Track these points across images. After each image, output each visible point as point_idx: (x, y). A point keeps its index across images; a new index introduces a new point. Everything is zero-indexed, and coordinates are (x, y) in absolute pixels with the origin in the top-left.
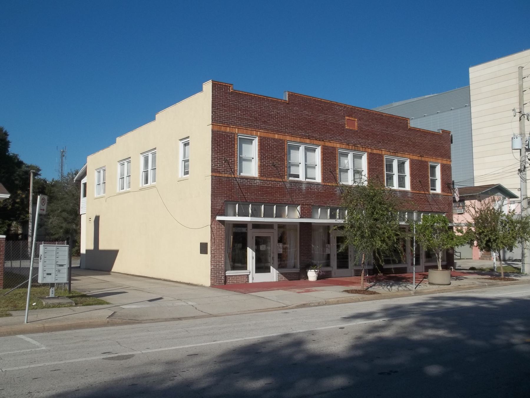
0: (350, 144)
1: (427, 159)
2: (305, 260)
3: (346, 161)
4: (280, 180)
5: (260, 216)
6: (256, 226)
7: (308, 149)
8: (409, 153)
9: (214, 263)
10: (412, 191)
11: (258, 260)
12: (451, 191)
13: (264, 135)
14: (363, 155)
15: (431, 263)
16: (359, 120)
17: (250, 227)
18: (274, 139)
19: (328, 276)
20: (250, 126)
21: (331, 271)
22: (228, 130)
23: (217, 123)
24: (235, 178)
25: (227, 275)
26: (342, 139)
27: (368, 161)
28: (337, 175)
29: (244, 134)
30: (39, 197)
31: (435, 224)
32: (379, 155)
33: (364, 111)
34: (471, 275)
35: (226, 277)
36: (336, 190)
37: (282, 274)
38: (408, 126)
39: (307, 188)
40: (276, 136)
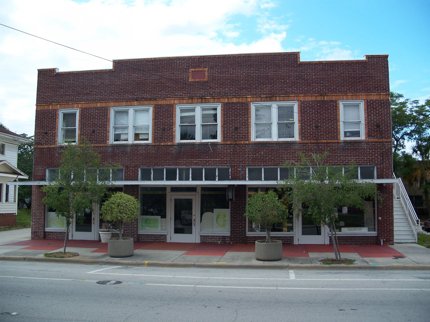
6: (175, 189)
9: (34, 220)
13: (85, 106)
16: (212, 68)
17: (168, 190)
21: (292, 237)
23: (41, 103)
28: (174, 133)
29: (65, 109)
30: (47, 172)
31: (312, 181)
35: (45, 232)
40: (99, 105)
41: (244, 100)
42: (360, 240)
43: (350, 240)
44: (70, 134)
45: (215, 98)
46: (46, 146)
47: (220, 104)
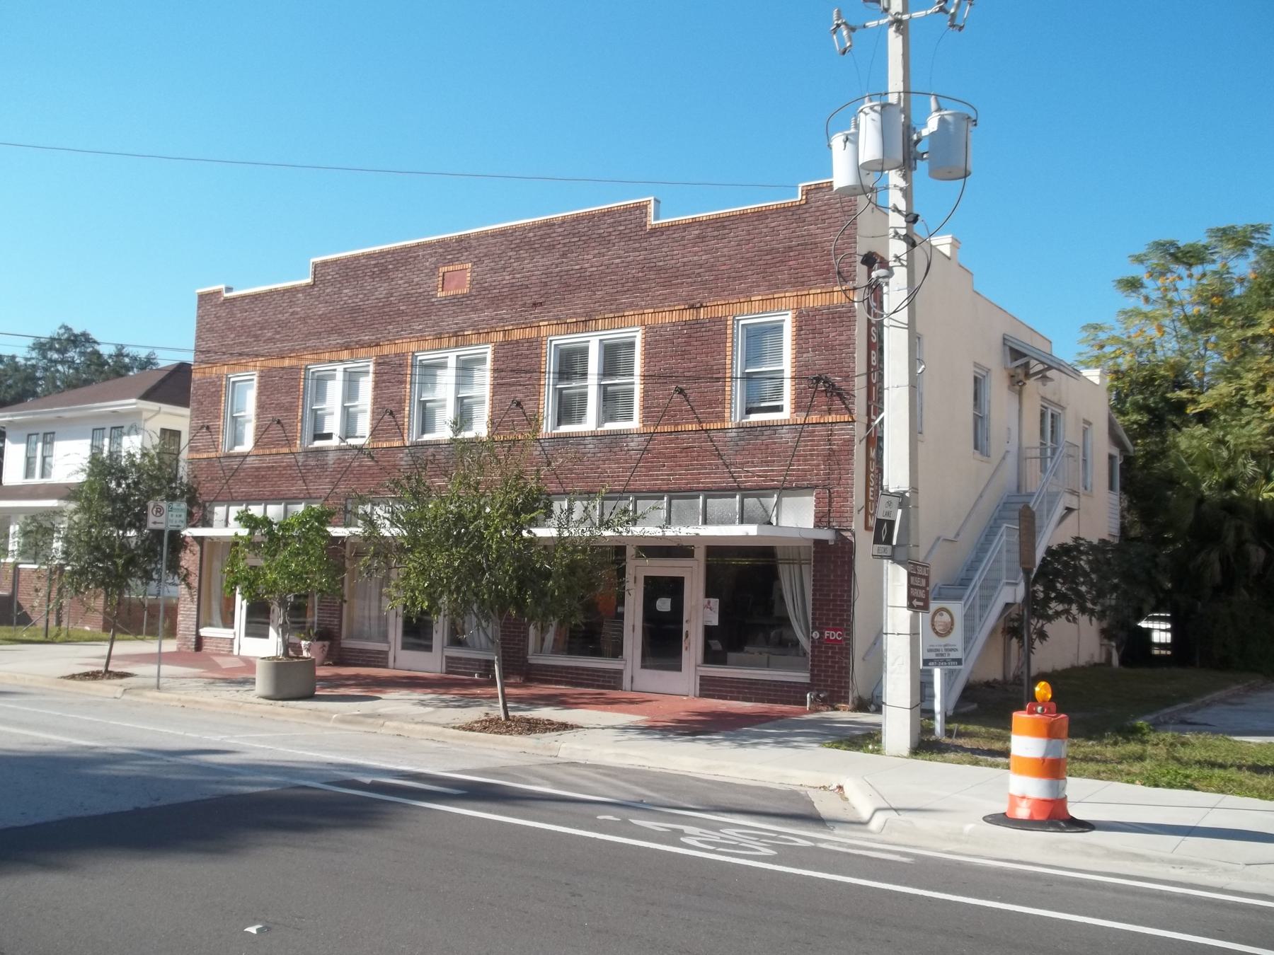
1: (720, 312)
4: (286, 450)
10: (255, 452)
11: (251, 612)
12: (844, 403)
15: (748, 671)
18: (283, 368)
19: (378, 662)
22: (702, 314)
32: (529, 341)
34: (733, 709)
41: (533, 333)
42: (769, 690)
43: (747, 688)
44: (612, 402)
45: (482, 333)
46: (205, 456)
47: (490, 346)
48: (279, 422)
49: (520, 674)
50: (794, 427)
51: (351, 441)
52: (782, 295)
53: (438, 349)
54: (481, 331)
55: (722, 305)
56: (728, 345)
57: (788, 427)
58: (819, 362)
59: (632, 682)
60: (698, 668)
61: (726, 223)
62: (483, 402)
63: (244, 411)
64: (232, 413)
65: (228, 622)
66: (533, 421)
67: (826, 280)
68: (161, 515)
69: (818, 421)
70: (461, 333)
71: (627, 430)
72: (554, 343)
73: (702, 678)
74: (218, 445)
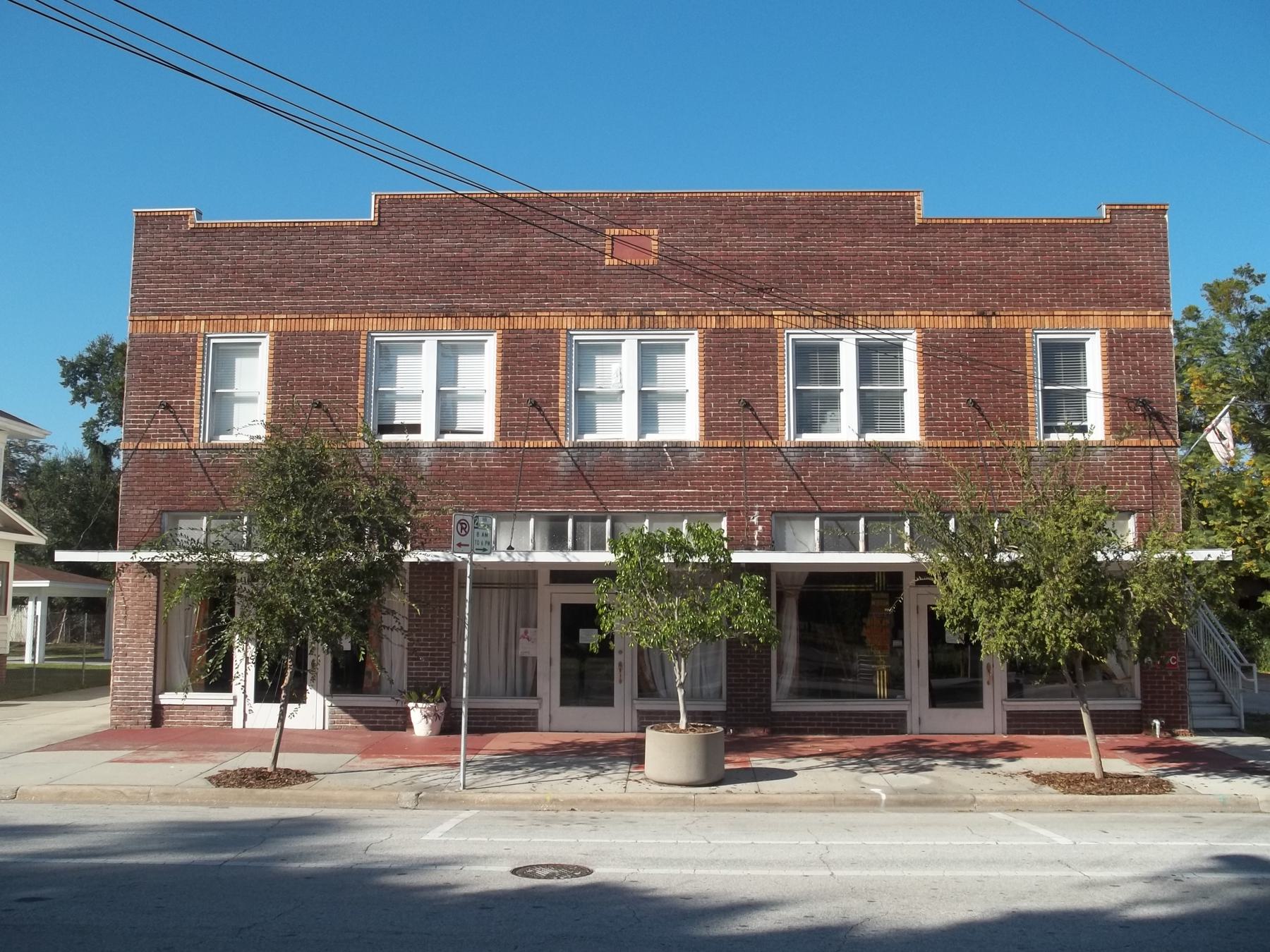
0: (621, 311)
1: (1017, 323)
2: (426, 674)
3: (615, 367)
5: (855, 549)
7: (602, 346)
8: (916, 311)
14: (1088, 339)
18: (324, 333)
20: (245, 308)
21: (535, 712)
24: (190, 449)
25: (163, 702)
26: (586, 301)
27: (703, 358)
32: (758, 332)
33: (690, 200)
36: (555, 459)
37: (345, 709)
38: (913, 218)
39: (439, 464)
40: (331, 325)
41: (763, 323)
46: (165, 445)
47: (696, 332)
48: (168, 407)
49: (762, 725)
50: (1110, 449)
51: (448, 438)
52: (1090, 313)
53: (611, 329)
54: (681, 313)
55: (1018, 316)
56: (198, 366)
57: (612, 450)
58: (1133, 384)
59: (550, 722)
60: (1004, 702)
61: (1016, 230)
62: (680, 398)
63: (233, 388)
64: (577, 386)
65: (222, 682)
66: (770, 431)
67: (1137, 304)
68: (467, 533)
69: (1139, 445)
70: (651, 313)
71: (906, 443)
72: (791, 337)
73: (1010, 714)
74: (191, 432)
